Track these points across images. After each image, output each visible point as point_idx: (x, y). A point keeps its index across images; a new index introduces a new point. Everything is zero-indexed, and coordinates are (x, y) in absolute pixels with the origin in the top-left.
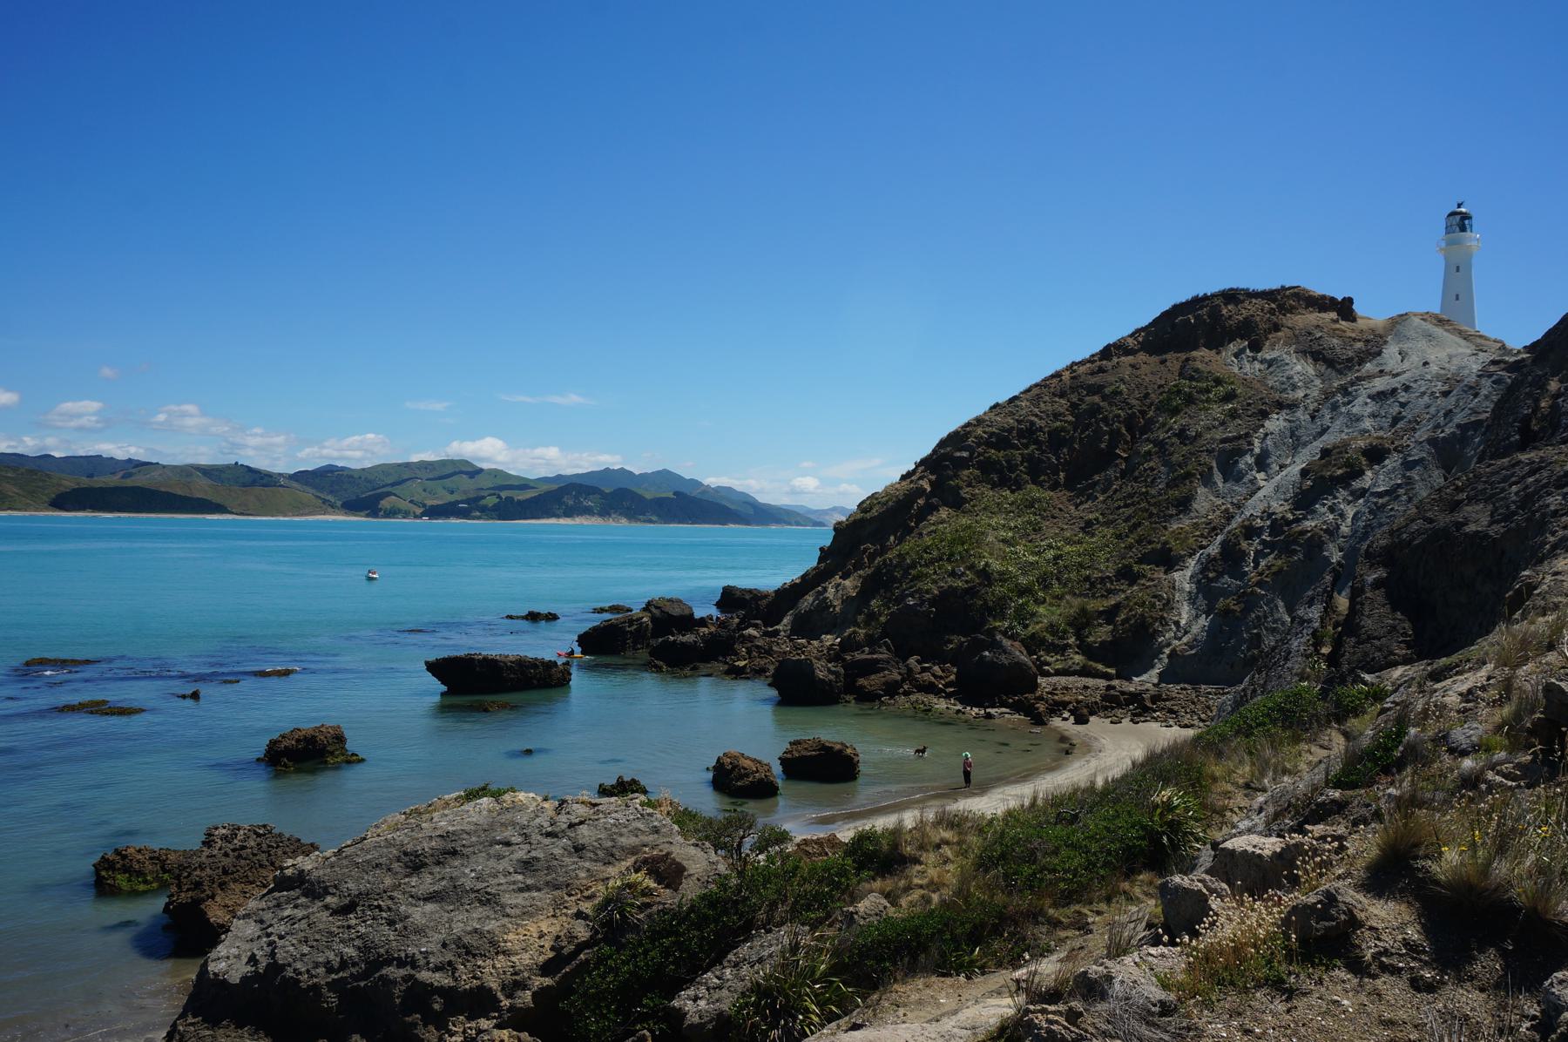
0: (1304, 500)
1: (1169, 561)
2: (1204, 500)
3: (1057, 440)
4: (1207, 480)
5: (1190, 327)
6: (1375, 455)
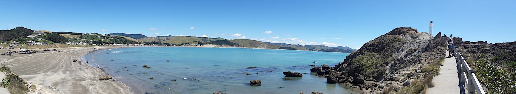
0: (405, 56)
1: (387, 64)
2: (394, 55)
3: (377, 46)
4: (395, 53)
5: (397, 31)
6: (415, 50)
